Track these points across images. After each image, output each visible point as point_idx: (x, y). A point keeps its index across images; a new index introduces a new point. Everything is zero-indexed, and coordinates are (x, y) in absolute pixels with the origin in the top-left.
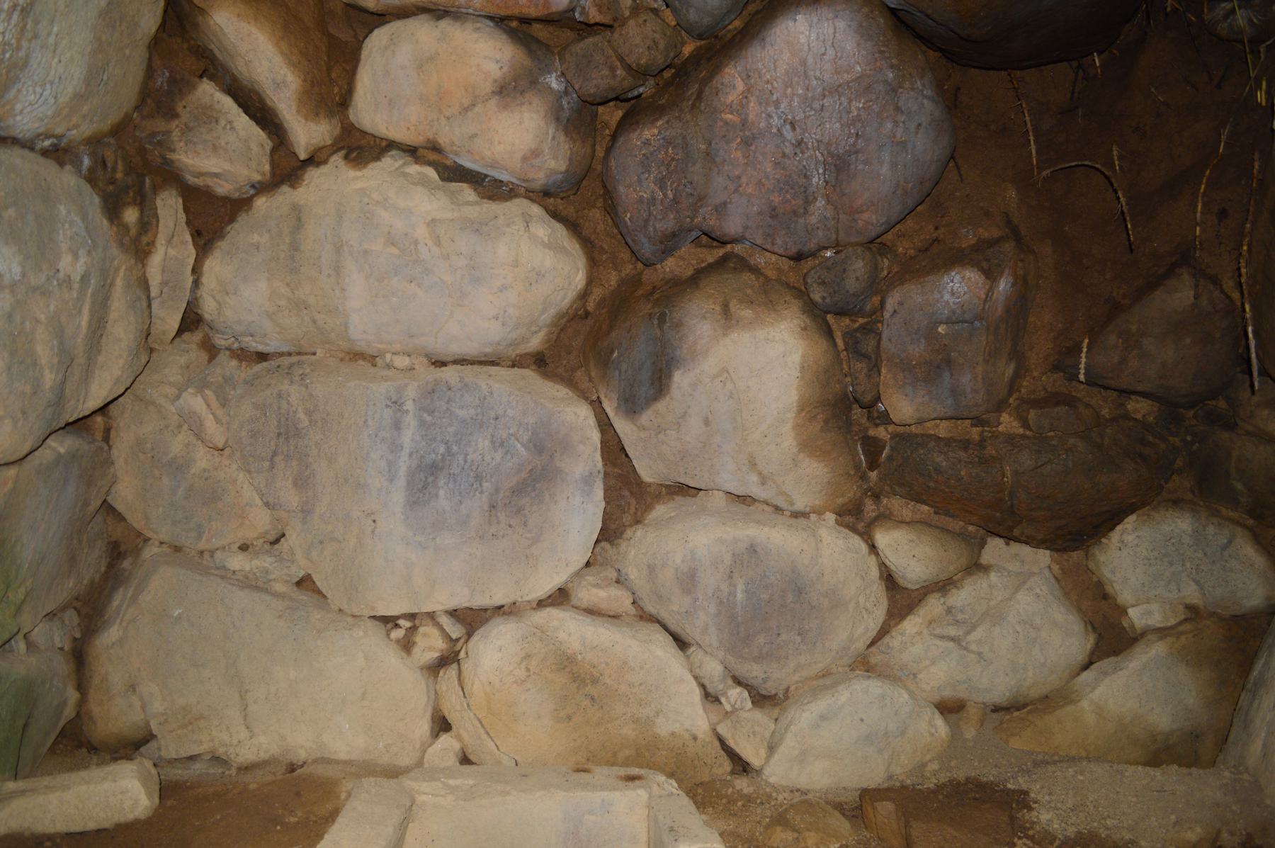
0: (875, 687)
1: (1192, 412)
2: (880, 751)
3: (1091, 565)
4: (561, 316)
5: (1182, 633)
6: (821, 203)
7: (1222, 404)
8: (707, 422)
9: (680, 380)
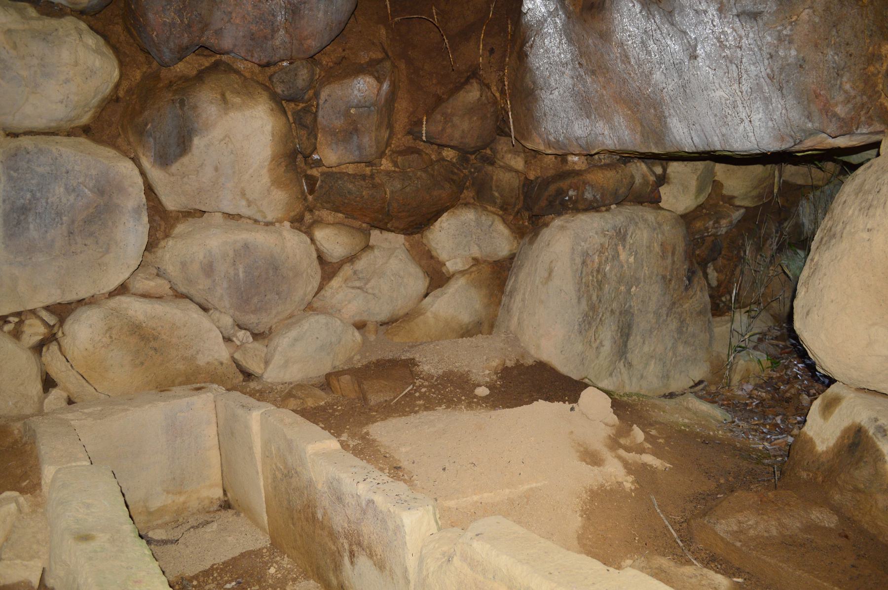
0: (322, 319)
1: (474, 156)
2: (328, 354)
3: (425, 241)
4: (103, 100)
5: (472, 272)
6: (282, 32)
7: (488, 151)
8: (216, 169)
9: (198, 142)
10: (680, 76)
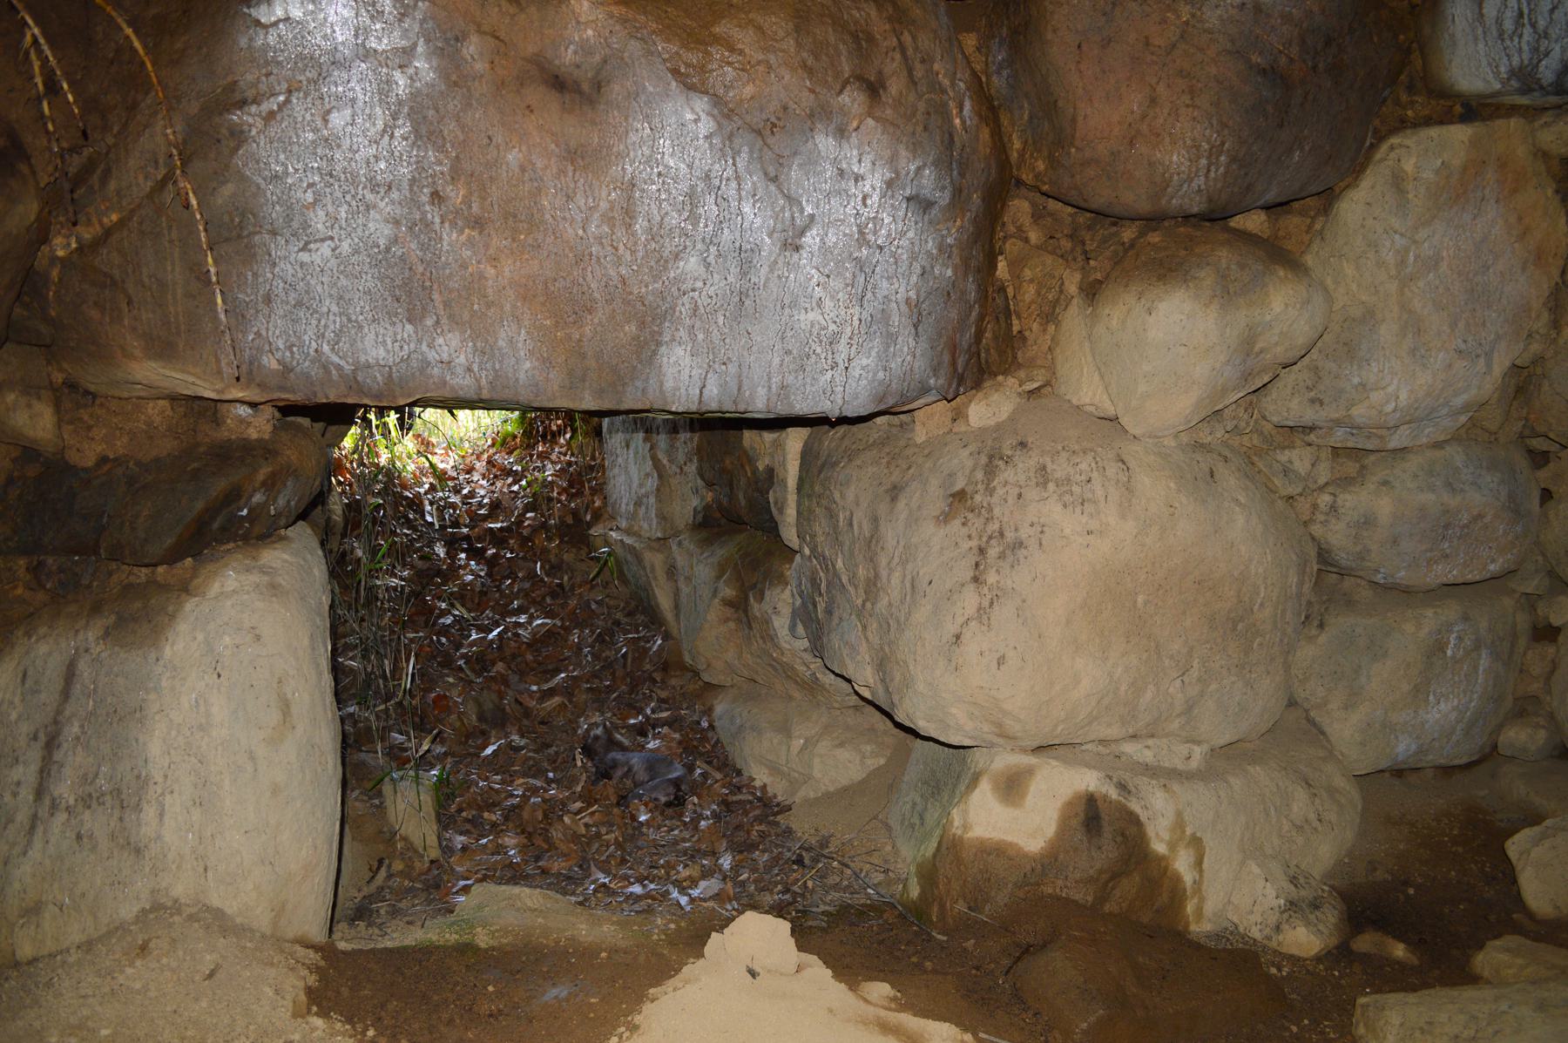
10: (744, 274)
